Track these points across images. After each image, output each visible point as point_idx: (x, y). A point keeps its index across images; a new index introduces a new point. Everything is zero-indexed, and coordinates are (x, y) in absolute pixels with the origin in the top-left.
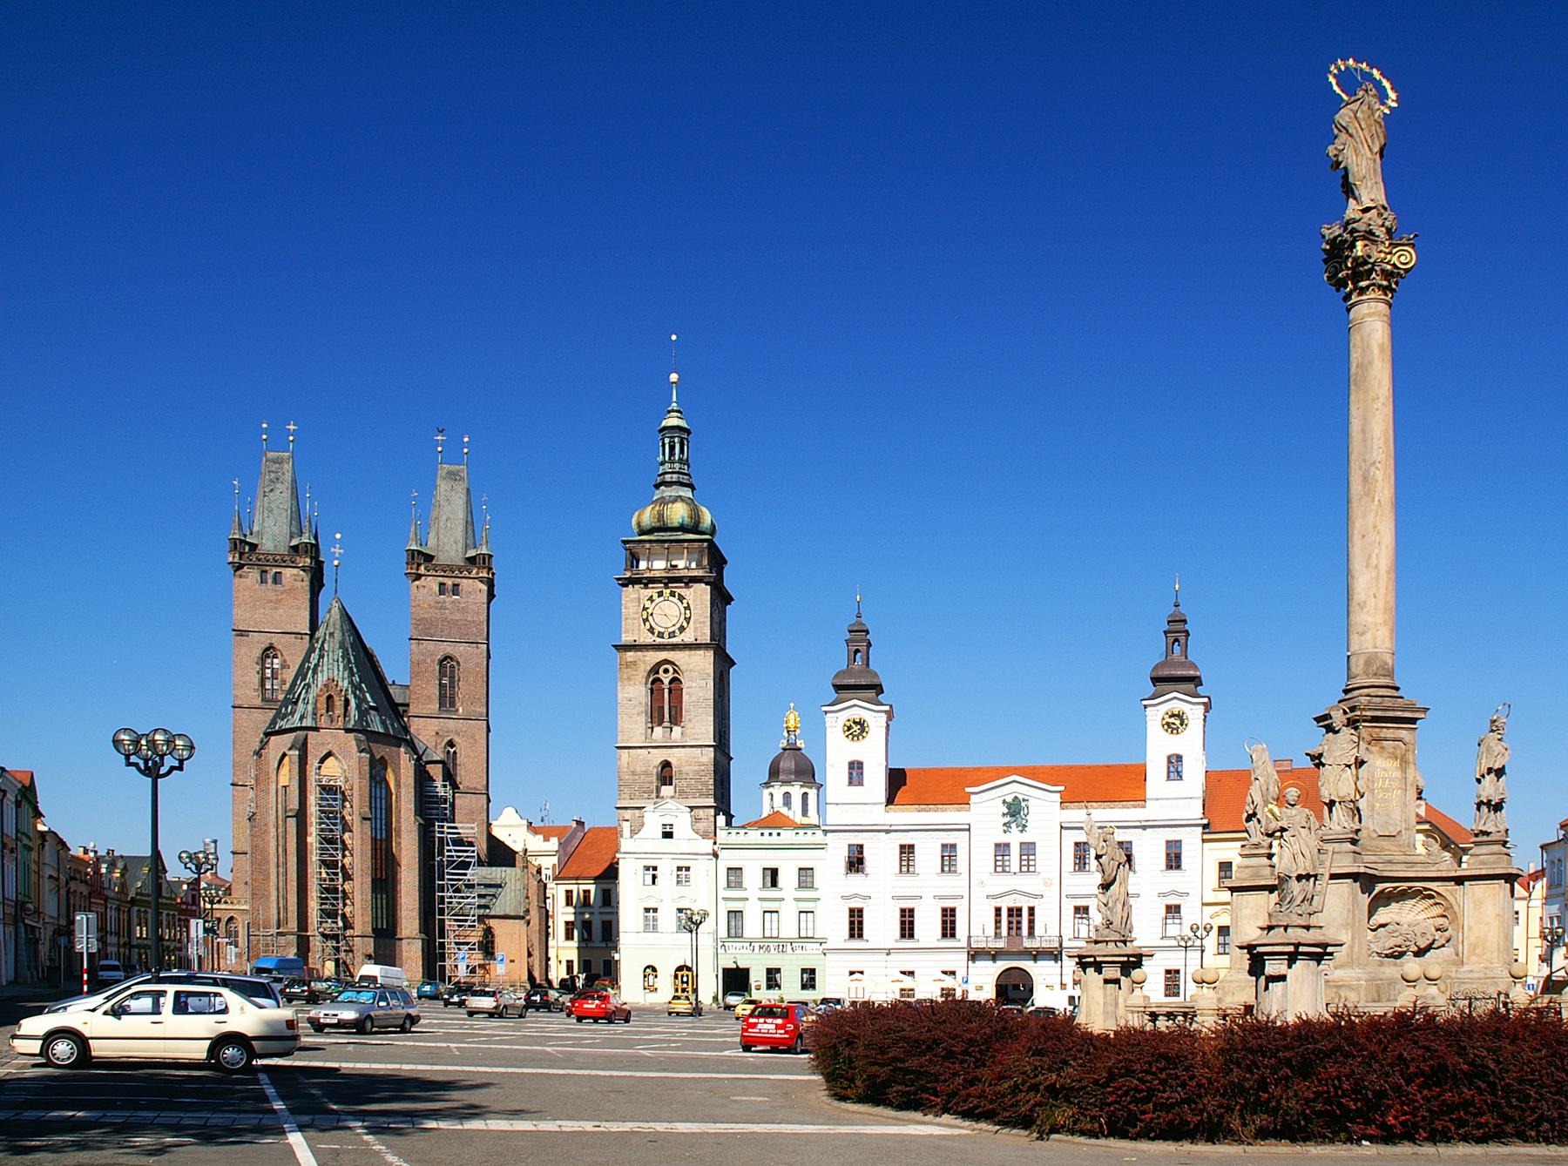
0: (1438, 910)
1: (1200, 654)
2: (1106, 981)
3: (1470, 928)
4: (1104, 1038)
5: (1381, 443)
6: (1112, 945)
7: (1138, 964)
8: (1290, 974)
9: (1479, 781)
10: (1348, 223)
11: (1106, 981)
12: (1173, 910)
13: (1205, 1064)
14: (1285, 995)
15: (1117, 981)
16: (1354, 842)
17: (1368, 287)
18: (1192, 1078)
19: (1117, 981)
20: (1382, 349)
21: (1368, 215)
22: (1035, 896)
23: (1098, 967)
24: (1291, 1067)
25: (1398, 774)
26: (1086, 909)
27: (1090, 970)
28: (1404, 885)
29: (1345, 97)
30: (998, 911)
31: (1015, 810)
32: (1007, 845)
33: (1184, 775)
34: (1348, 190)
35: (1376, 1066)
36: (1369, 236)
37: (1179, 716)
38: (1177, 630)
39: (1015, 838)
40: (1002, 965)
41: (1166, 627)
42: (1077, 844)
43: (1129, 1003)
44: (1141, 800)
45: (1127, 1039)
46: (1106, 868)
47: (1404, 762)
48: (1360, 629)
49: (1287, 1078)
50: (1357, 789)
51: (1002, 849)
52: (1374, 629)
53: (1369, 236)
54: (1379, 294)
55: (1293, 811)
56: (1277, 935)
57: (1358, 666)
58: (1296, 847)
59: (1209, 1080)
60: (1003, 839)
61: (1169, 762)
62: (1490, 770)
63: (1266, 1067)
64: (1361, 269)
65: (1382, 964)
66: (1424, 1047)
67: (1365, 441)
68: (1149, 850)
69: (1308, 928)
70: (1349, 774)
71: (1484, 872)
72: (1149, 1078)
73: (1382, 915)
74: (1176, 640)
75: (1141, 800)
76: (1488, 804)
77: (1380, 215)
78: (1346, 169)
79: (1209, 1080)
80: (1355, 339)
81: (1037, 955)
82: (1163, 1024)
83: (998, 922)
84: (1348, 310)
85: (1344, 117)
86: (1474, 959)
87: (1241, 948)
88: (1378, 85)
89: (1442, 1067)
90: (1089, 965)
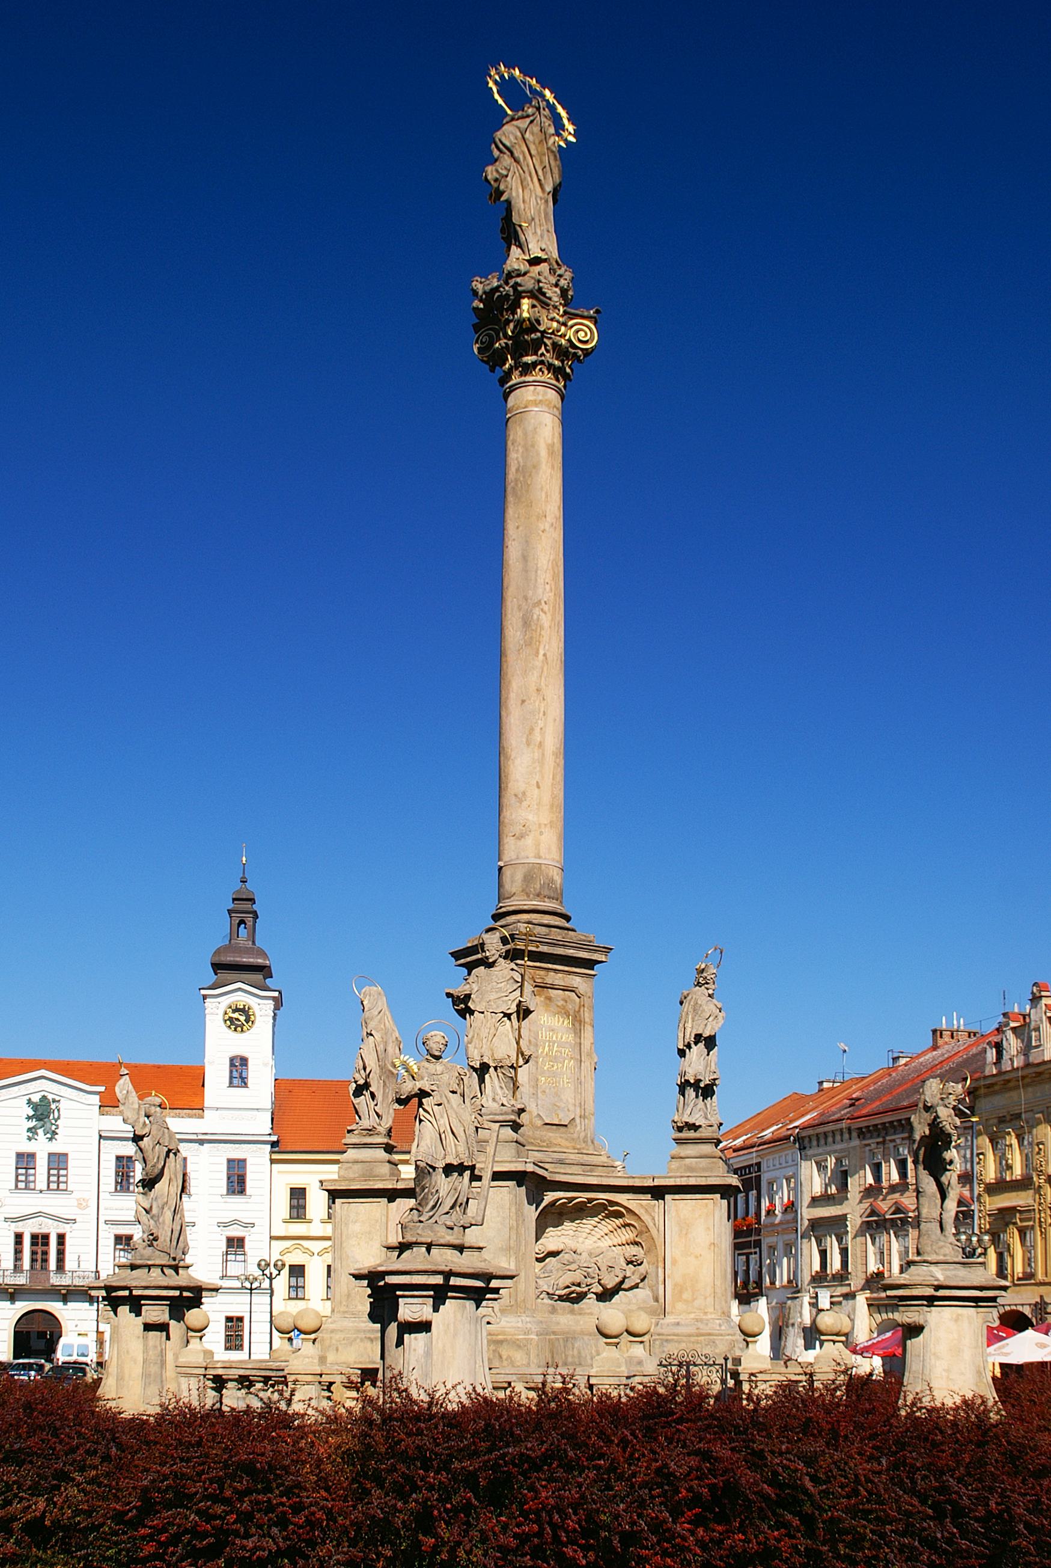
0: (628, 1235)
1: (270, 940)
2: (148, 1327)
3: (674, 1262)
4: (137, 1425)
5: (548, 577)
6: (156, 1272)
7: (195, 1302)
8: (437, 1319)
9: (682, 1053)
10: (509, 275)
11: (148, 1327)
12: (236, 1244)
13: (323, 1483)
14: (428, 1353)
15: (163, 1327)
16: (516, 1127)
17: (534, 365)
18: (297, 1508)
19: (163, 1327)
20: (551, 453)
21: (537, 269)
22: (68, 1221)
23: (136, 1304)
24: (474, 1488)
25: (570, 1038)
26: (129, 1238)
27: (124, 1310)
28: (583, 1196)
29: (509, 112)
30: (19, 1238)
31: (43, 1113)
32: (32, 1156)
33: (250, 1082)
34: (511, 235)
35: (619, 1487)
36: (538, 295)
37: (244, 1011)
38: (243, 910)
39: (42, 1147)
40: (23, 1307)
41: (231, 906)
42: (119, 1158)
43: (182, 1360)
44: (197, 1108)
45: (180, 1432)
46: (149, 1155)
47: (578, 1023)
48: (517, 829)
49: (467, 1507)
50: (520, 1052)
51: (26, 1161)
52: (535, 827)
53: (538, 295)
54: (548, 377)
55: (438, 1067)
56: (414, 1259)
57: (513, 881)
58: (443, 1122)
59: (329, 1513)
60: (27, 1147)
61: (232, 1064)
62: (698, 1038)
63: (431, 1488)
64: (527, 339)
65: (554, 1310)
66: (697, 1453)
67: (526, 570)
68: (206, 1168)
69: (460, 1248)
70: (507, 1027)
71: (692, 1182)
72: (219, 1509)
73: (554, 1238)
74: (242, 922)
75: (197, 1108)
76: (696, 1085)
77: (552, 271)
78: (508, 202)
79: (329, 1513)
80: (515, 433)
81: (67, 1295)
82: (234, 1399)
83: (18, 1252)
84: (506, 396)
85: (508, 134)
86: (680, 1306)
87: (357, 1277)
88: (552, 108)
89: (731, 1490)
90: (122, 1301)
